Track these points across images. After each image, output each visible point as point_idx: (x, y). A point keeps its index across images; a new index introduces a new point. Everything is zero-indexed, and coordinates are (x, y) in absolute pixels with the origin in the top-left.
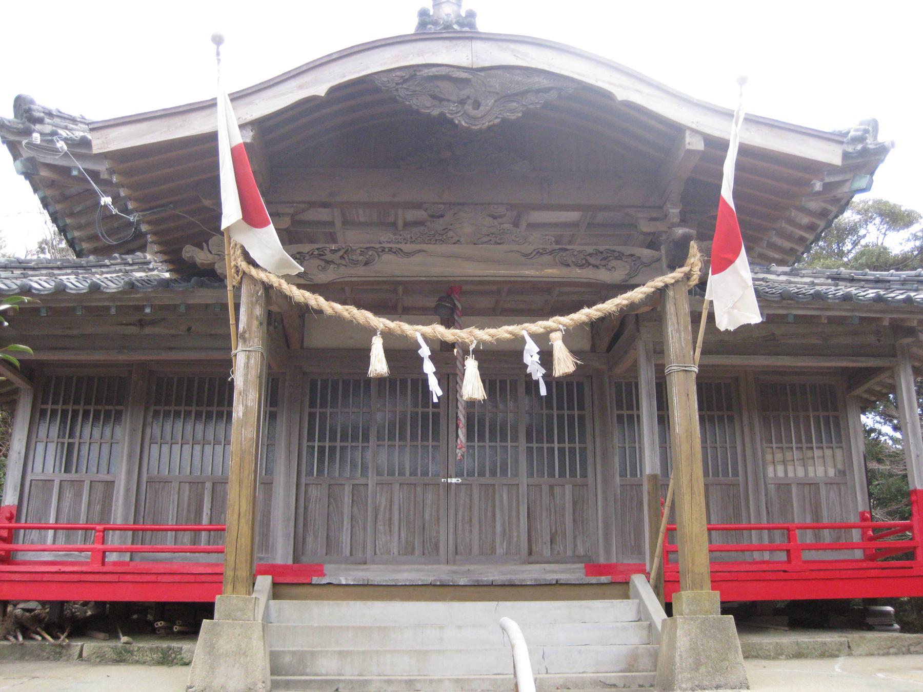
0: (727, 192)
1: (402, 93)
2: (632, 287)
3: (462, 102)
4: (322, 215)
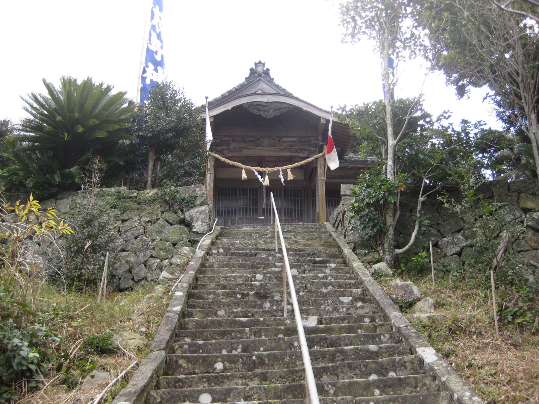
0: (330, 133)
1: (250, 109)
2: (309, 158)
3: (265, 111)
4: (227, 139)
